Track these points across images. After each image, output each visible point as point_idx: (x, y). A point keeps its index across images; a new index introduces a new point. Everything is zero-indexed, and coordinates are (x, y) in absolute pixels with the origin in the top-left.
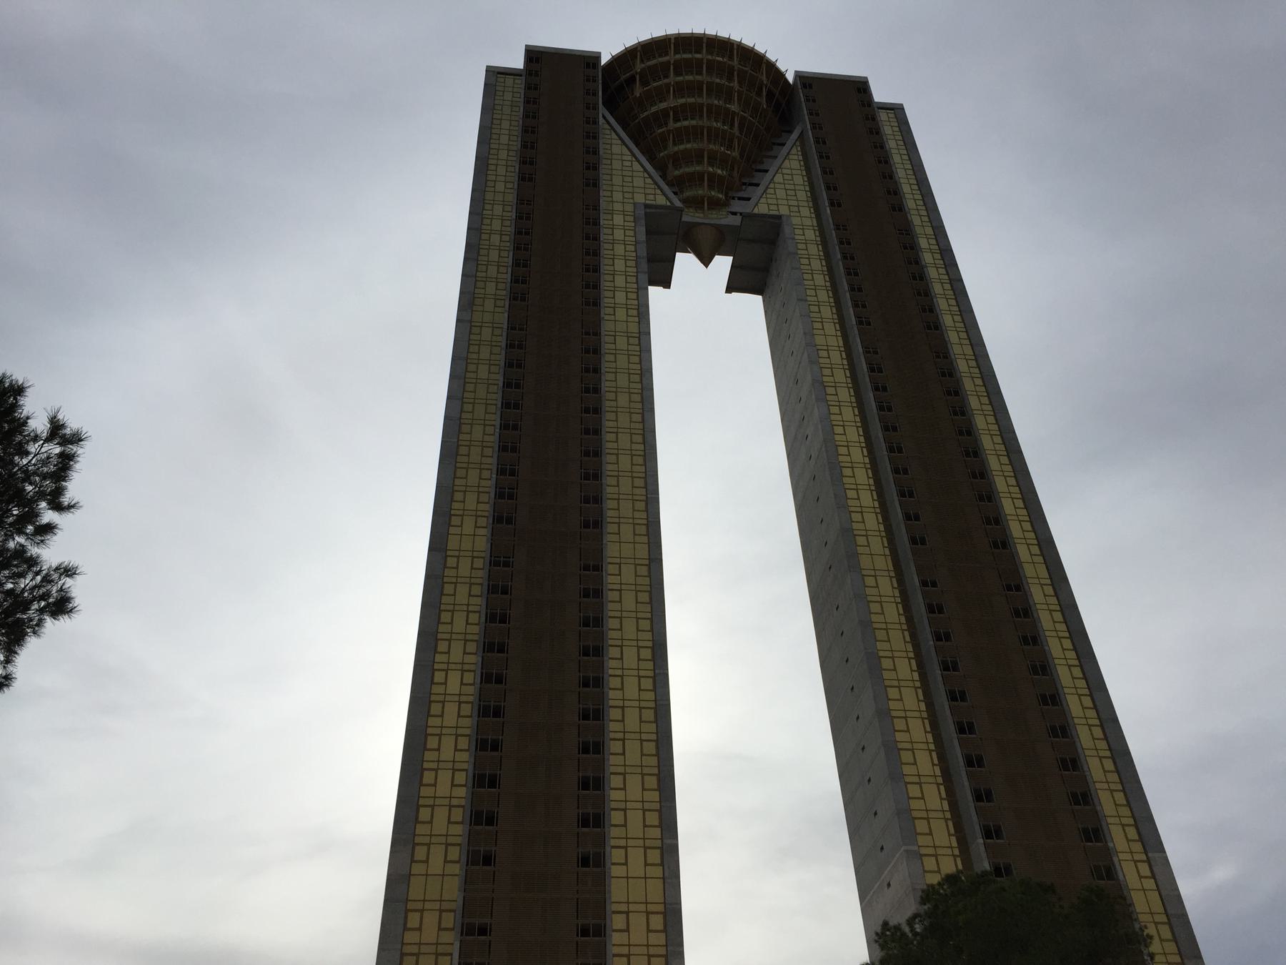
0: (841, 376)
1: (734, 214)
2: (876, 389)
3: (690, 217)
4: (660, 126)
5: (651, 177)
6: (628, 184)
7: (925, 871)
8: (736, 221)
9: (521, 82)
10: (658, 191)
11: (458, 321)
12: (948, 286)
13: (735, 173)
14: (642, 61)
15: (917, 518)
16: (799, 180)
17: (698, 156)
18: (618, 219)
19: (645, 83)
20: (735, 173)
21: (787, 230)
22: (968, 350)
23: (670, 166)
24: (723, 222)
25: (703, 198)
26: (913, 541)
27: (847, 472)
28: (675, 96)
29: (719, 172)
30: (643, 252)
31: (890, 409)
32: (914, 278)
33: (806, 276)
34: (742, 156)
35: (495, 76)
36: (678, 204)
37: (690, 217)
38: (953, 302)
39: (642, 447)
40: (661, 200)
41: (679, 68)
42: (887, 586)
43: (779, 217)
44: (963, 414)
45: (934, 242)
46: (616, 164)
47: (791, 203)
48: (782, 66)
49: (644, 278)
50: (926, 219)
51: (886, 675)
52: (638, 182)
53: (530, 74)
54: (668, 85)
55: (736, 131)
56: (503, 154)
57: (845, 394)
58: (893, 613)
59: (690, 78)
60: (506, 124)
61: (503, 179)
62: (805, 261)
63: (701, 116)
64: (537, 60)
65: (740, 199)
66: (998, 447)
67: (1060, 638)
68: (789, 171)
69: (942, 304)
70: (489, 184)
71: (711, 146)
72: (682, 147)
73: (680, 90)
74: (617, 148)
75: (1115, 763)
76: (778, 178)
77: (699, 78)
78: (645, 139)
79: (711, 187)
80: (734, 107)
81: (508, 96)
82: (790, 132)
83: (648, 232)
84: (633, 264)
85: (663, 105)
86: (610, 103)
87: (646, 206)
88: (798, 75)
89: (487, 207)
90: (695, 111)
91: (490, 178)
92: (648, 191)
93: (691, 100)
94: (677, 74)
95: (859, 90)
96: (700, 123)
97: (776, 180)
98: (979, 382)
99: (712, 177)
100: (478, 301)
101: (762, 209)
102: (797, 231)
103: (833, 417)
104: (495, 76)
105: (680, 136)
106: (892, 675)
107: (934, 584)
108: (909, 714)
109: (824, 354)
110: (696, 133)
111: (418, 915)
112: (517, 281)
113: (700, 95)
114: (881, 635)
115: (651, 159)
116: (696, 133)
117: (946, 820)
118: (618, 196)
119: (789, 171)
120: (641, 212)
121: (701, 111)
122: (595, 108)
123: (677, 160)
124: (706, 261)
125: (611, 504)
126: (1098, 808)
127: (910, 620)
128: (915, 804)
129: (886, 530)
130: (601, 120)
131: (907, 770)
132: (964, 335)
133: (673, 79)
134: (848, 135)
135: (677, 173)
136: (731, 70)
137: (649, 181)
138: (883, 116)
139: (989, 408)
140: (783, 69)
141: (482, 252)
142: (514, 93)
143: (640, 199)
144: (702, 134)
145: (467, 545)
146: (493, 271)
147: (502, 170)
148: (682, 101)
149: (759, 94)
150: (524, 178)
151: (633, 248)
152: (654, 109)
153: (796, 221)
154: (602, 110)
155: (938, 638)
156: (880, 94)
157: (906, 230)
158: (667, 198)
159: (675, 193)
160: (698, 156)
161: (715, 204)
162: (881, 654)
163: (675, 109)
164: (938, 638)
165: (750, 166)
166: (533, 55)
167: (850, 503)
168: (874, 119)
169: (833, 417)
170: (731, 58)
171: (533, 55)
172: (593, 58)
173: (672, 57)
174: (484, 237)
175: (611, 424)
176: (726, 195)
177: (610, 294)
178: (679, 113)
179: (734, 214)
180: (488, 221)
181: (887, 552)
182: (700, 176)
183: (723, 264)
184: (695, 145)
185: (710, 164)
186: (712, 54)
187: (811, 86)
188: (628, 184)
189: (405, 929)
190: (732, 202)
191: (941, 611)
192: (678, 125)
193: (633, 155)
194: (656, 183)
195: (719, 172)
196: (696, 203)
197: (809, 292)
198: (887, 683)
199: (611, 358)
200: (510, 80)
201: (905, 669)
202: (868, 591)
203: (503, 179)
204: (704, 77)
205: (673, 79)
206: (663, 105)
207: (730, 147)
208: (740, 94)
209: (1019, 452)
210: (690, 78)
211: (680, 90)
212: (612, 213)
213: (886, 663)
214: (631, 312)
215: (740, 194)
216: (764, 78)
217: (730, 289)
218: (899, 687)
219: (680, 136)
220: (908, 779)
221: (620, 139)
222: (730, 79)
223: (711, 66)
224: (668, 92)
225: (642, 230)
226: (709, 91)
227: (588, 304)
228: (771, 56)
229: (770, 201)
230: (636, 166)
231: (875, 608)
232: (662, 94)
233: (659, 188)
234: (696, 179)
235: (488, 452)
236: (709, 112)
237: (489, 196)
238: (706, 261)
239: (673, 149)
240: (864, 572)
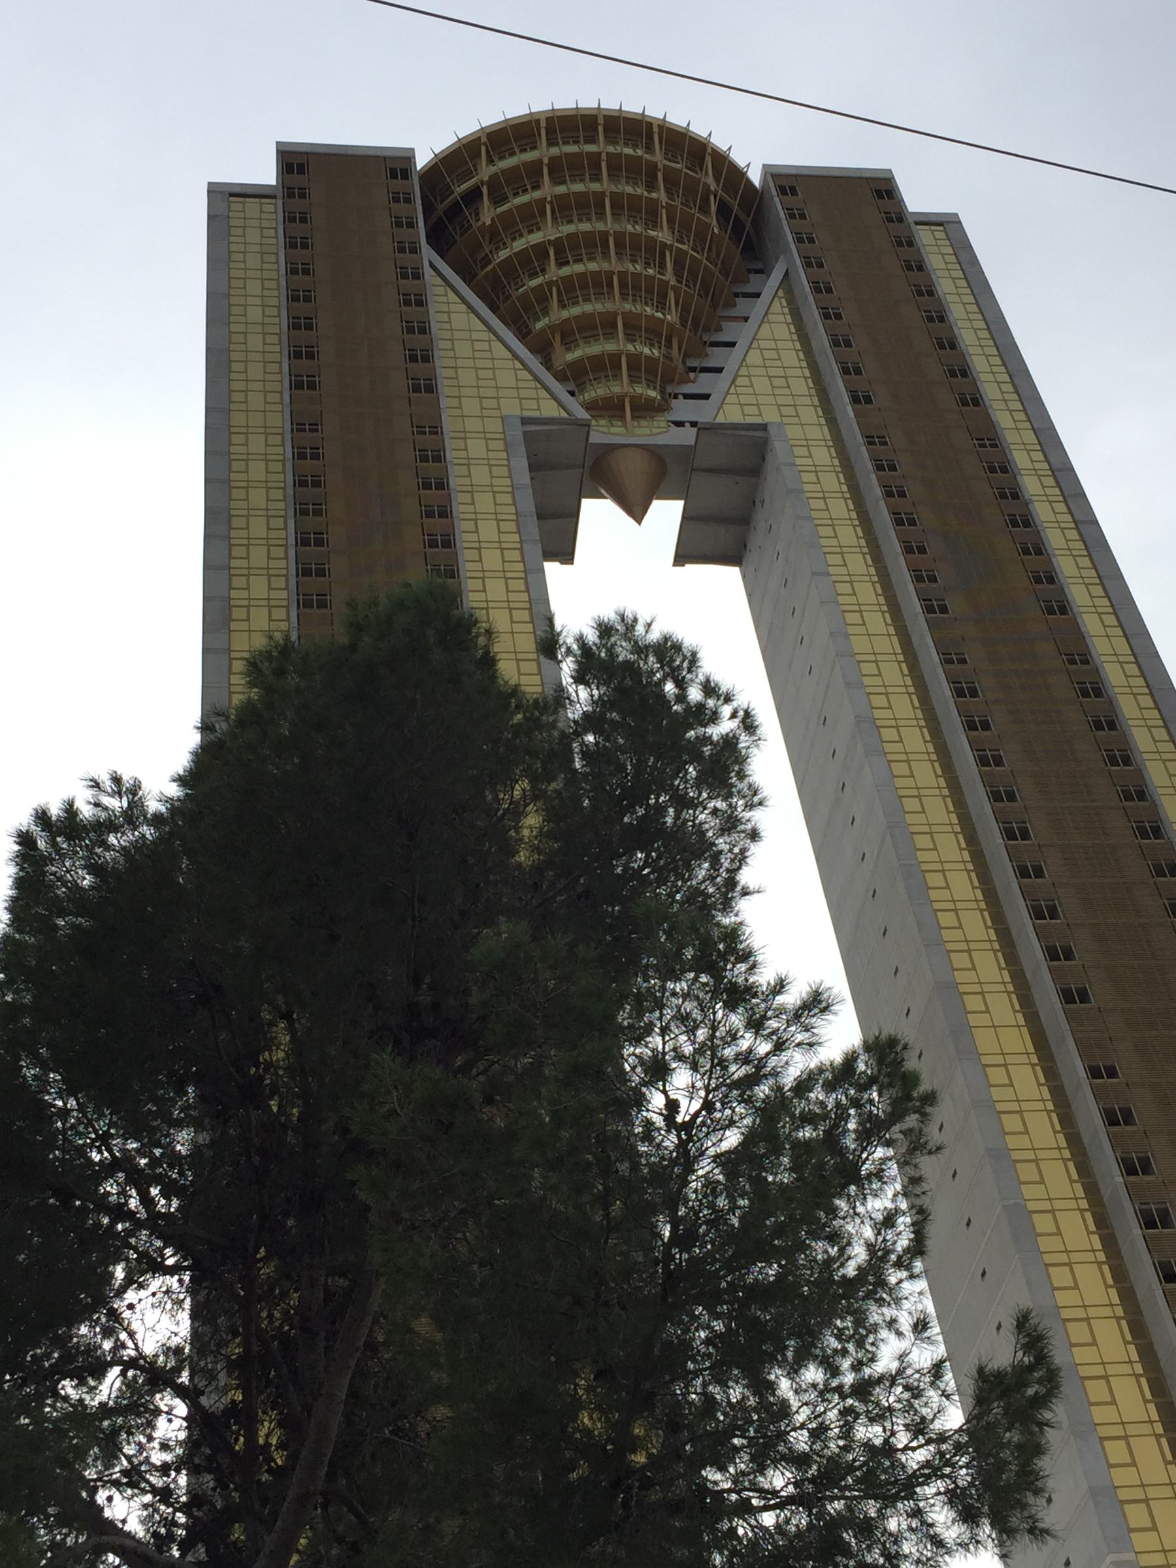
1: (680, 424)
3: (604, 433)
5: (526, 367)
6: (488, 385)
7: (1111, 1466)
8: (687, 436)
9: (273, 212)
10: (543, 393)
13: (675, 352)
16: (792, 357)
17: (608, 325)
18: (477, 448)
20: (675, 352)
23: (557, 342)
24: (661, 440)
25: (621, 399)
26: (1067, 997)
27: (935, 880)
30: (528, 504)
32: (910, 268)
33: (823, 531)
35: (226, 201)
36: (583, 414)
37: (604, 433)
39: (525, 596)
40: (550, 409)
41: (559, 170)
42: (1028, 1083)
43: (764, 427)
44: (1127, 761)
45: (1039, 456)
46: (462, 349)
47: (781, 400)
48: (739, 158)
51: (1044, 1243)
52: (506, 378)
53: (291, 195)
54: (541, 202)
55: (669, 276)
56: (255, 342)
58: (1044, 1130)
60: (254, 288)
61: (259, 386)
62: (817, 504)
63: (606, 255)
64: (301, 169)
65: (687, 396)
66: (1098, 602)
67: (1062, 529)
68: (772, 345)
70: (236, 397)
71: (628, 306)
72: (575, 311)
73: (564, 208)
74: (461, 318)
76: (754, 357)
77: (595, 186)
78: (503, 295)
79: (634, 380)
80: (663, 235)
81: (253, 236)
82: (764, 272)
83: (532, 468)
84: (512, 526)
85: (536, 238)
86: (439, 239)
87: (525, 421)
88: (772, 173)
89: (236, 439)
90: (594, 244)
91: (235, 386)
92: (523, 393)
93: (585, 227)
94: (557, 180)
96: (605, 266)
97: (749, 360)
98: (1147, 701)
99: (635, 362)
100: (237, 613)
101: (732, 414)
102: (798, 451)
103: (899, 782)
104: (226, 201)
105: (570, 290)
107: (1112, 1073)
109: (844, 588)
110: (598, 285)
111: (243, 442)
112: (306, 572)
113: (601, 216)
114: (1027, 1172)
115: (523, 334)
116: (598, 285)
117: (981, 911)
118: (470, 406)
119: (772, 345)
120: (517, 433)
121: (605, 245)
122: (415, 250)
123: (568, 334)
124: (637, 511)
125: (468, 555)
126: (1083, 630)
128: (1120, 1477)
129: (904, 653)
130: (428, 272)
131: (1099, 1414)
132: (1111, 620)
134: (871, 272)
135: (570, 357)
136: (652, 169)
137: (525, 375)
138: (924, 236)
139: (1106, 602)
140: (741, 162)
141: (236, 522)
142: (264, 231)
143: (511, 408)
144: (610, 285)
147: (255, 371)
149: (704, 209)
152: (519, 245)
153: (793, 432)
154: (428, 253)
155: (1129, 1170)
156: (917, 199)
157: (988, 440)
158: (561, 405)
159: (572, 394)
161: (644, 409)
162: (1032, 1206)
163: (558, 244)
164: (1130, 1171)
166: (294, 161)
168: (911, 244)
169: (899, 782)
170: (649, 148)
173: (543, 152)
174: (236, 494)
176: (662, 392)
178: (565, 250)
179: (680, 424)
180: (241, 523)
181: (892, 630)
182: (614, 361)
183: (667, 514)
184: (599, 307)
185: (630, 338)
186: (614, 142)
187: (793, 191)
188: (488, 385)
189: (231, 499)
190: (674, 403)
191: (1128, 1119)
192: (566, 271)
193: (490, 329)
194: (537, 379)
196: (611, 408)
198: (1048, 1259)
199: (478, 584)
200: (252, 206)
201: (1077, 1231)
202: (996, 1094)
203: (259, 386)
204: (605, 185)
205: (549, 189)
206: (536, 238)
207: (662, 305)
208: (670, 210)
211: (564, 208)
212: (464, 436)
213: (1043, 1223)
215: (689, 389)
216: (710, 180)
217: (681, 559)
219: (570, 290)
220: (1103, 1431)
221: (464, 301)
223: (618, 203)
225: (521, 463)
226: (617, 207)
227: (417, 389)
228: (720, 142)
229: (743, 399)
230: (499, 350)
231: (1011, 1123)
232: (530, 217)
234: (605, 366)
236: (620, 245)
237: (238, 419)
238: (637, 511)
239: (558, 314)
240: (985, 1060)
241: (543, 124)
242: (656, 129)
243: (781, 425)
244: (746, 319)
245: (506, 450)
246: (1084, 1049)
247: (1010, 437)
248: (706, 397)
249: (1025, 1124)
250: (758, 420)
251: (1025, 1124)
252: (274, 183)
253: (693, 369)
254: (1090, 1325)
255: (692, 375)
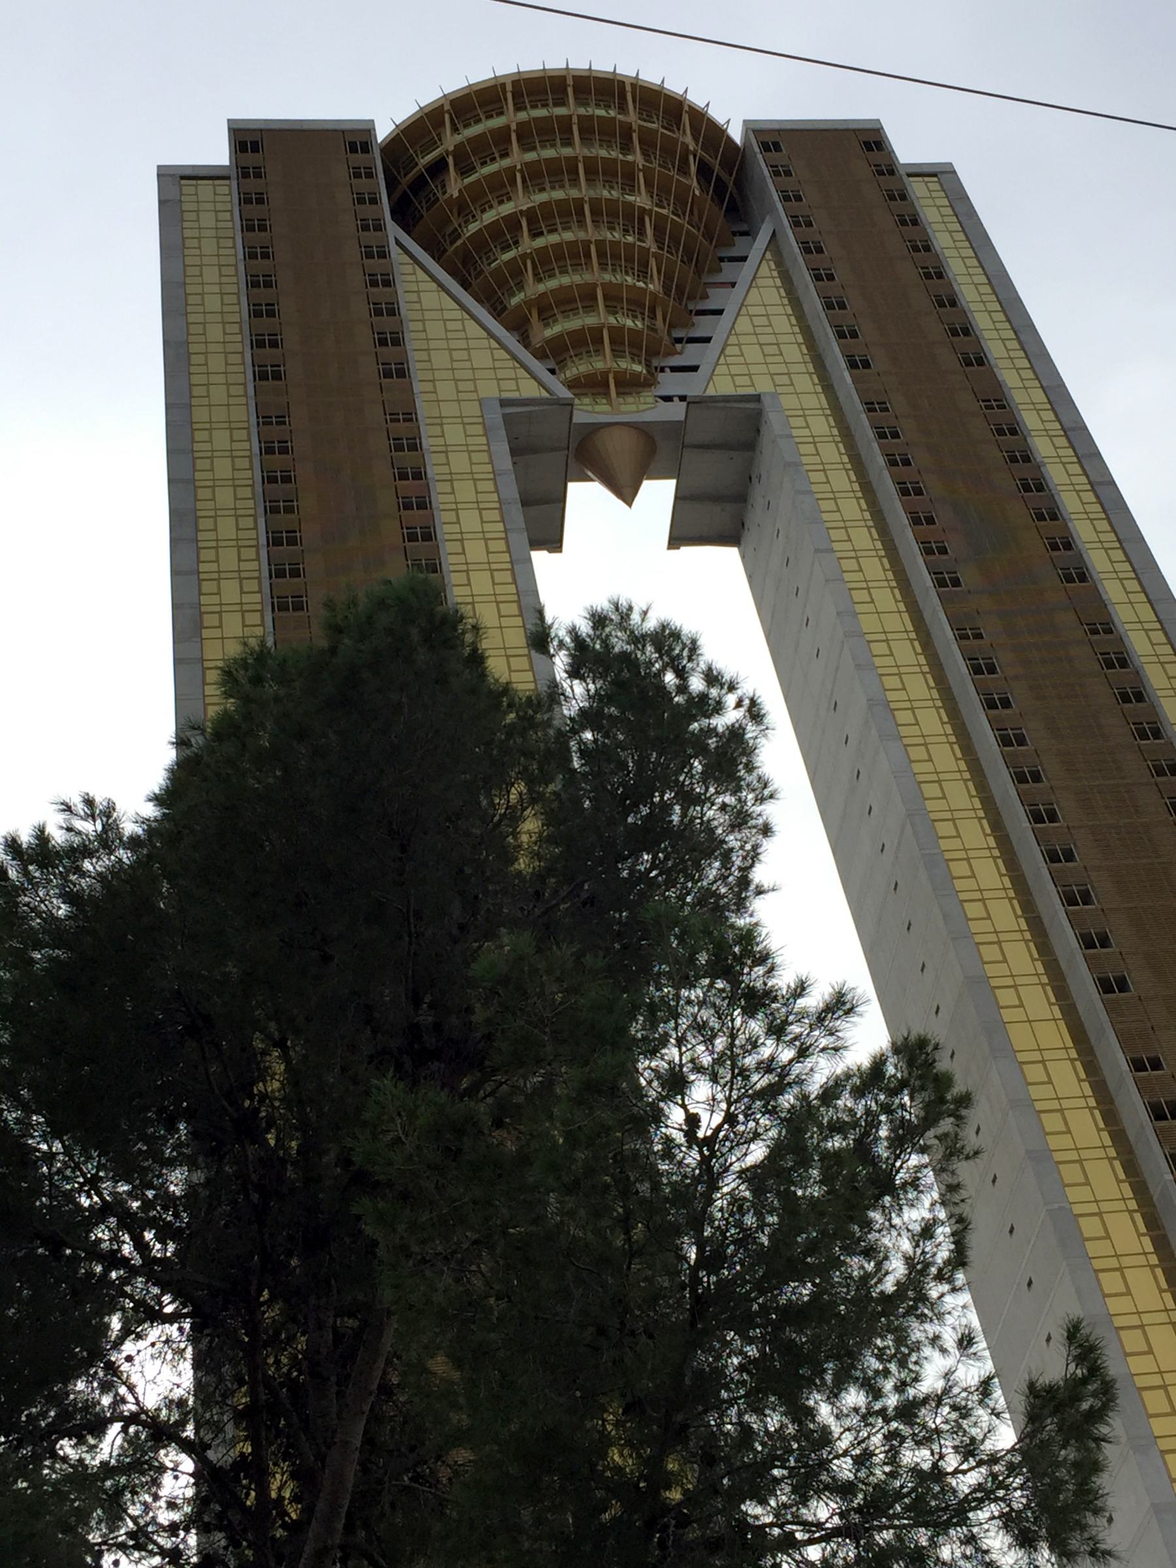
0: (920, 687)
1: (668, 399)
2: (990, 704)
3: (588, 412)
4: (506, 248)
6: (462, 363)
8: (676, 412)
9: (228, 193)
10: (522, 373)
11: (177, 662)
12: (1089, 497)
14: (455, 130)
15: (1105, 942)
16: (783, 322)
17: (586, 298)
19: (465, 170)
21: (773, 420)
22: (1146, 613)
24: (648, 417)
25: (605, 374)
26: (1105, 986)
27: (959, 869)
28: (508, 127)
29: (629, 323)
30: (512, 492)
31: (1021, 741)
34: (667, 290)
35: (178, 185)
36: (564, 393)
37: (588, 412)
38: (1104, 525)
40: (530, 389)
41: (527, 135)
42: (1067, 1078)
43: (757, 398)
45: (1050, 416)
46: (435, 329)
47: (774, 369)
48: (718, 114)
49: (520, 539)
50: (1029, 374)
51: (1092, 1248)
52: (482, 359)
53: (245, 175)
54: (511, 171)
55: (650, 243)
57: (933, 721)
58: (1087, 1128)
59: (549, 153)
60: (211, 275)
62: (818, 477)
63: (581, 223)
64: (255, 147)
65: (674, 369)
66: (1061, 452)
69: (1070, 503)
70: (197, 391)
71: (608, 277)
72: (552, 284)
73: (535, 176)
74: (432, 298)
75: (1029, 361)
76: (743, 324)
79: (617, 354)
80: (641, 200)
81: (208, 220)
83: (514, 452)
84: (495, 515)
85: (507, 209)
86: (404, 214)
87: (504, 403)
88: (754, 129)
90: (570, 213)
92: (501, 374)
93: (559, 194)
94: (526, 146)
95: (868, 146)
96: (582, 235)
97: (739, 328)
99: (617, 336)
100: (209, 620)
101: (722, 386)
102: (794, 422)
103: (917, 768)
104: (178, 185)
105: (545, 263)
106: (1065, 1141)
108: (1085, 1154)
110: (576, 255)
112: (269, 451)
114: (1071, 1173)
115: (498, 310)
116: (576, 255)
118: (446, 390)
120: (496, 416)
122: (379, 227)
123: (546, 309)
124: (626, 492)
127: (1119, 1138)
129: (1030, 929)
130: (394, 250)
132: (1133, 585)
133: (518, 157)
134: (858, 221)
135: (549, 333)
136: (627, 131)
137: (503, 354)
138: (917, 189)
142: (219, 212)
143: (489, 390)
144: (588, 255)
145: (220, 414)
146: (229, 559)
148: (542, 197)
149: (684, 170)
150: (266, 373)
151: (490, 486)
152: (489, 217)
153: (788, 402)
154: (393, 230)
156: (909, 148)
157: (996, 400)
158: (541, 384)
159: (553, 372)
160: (586, 298)
161: (629, 385)
162: (1077, 1209)
163: (531, 215)
165: (681, 308)
166: (247, 139)
167: (974, 927)
169: (917, 768)
170: (623, 108)
171: (247, 139)
172: (355, 138)
173: (511, 118)
174: (202, 493)
175: (438, 469)
176: (648, 366)
177: (451, 516)
178: (538, 221)
179: (668, 399)
180: (206, 464)
182: (595, 336)
183: (658, 494)
186: (586, 104)
188: (462, 363)
190: (661, 377)
192: (540, 242)
193: (463, 307)
194: (514, 358)
195: (629, 323)
196: (594, 385)
197: (834, 534)
198: (1097, 1264)
200: (205, 188)
204: (577, 150)
206: (507, 209)
207: (643, 274)
208: (647, 172)
209: (1096, 454)
210: (549, 153)
211: (535, 176)
213: (1090, 1227)
214: (482, 486)
218: (1120, 1269)
219: (545, 263)
222: (626, 148)
224: (513, 182)
225: (502, 448)
226: (591, 171)
228: (697, 98)
229: (735, 370)
230: (472, 328)
231: (1052, 1122)
232: (500, 187)
233: (524, 366)
235: (252, 585)
236: (596, 212)
237: (200, 414)
238: (626, 492)
239: (534, 289)
240: (1021, 1057)
241: (509, 88)
242: (628, 88)
243: (775, 395)
244: (733, 285)
245: (485, 435)
246: (1125, 1041)
247: (1018, 397)
248: (694, 369)
249: (1066, 1123)
250: (750, 391)
251: (1066, 1123)
252: (227, 163)
253: (679, 340)
254: (914, 713)
255: (678, 346)
